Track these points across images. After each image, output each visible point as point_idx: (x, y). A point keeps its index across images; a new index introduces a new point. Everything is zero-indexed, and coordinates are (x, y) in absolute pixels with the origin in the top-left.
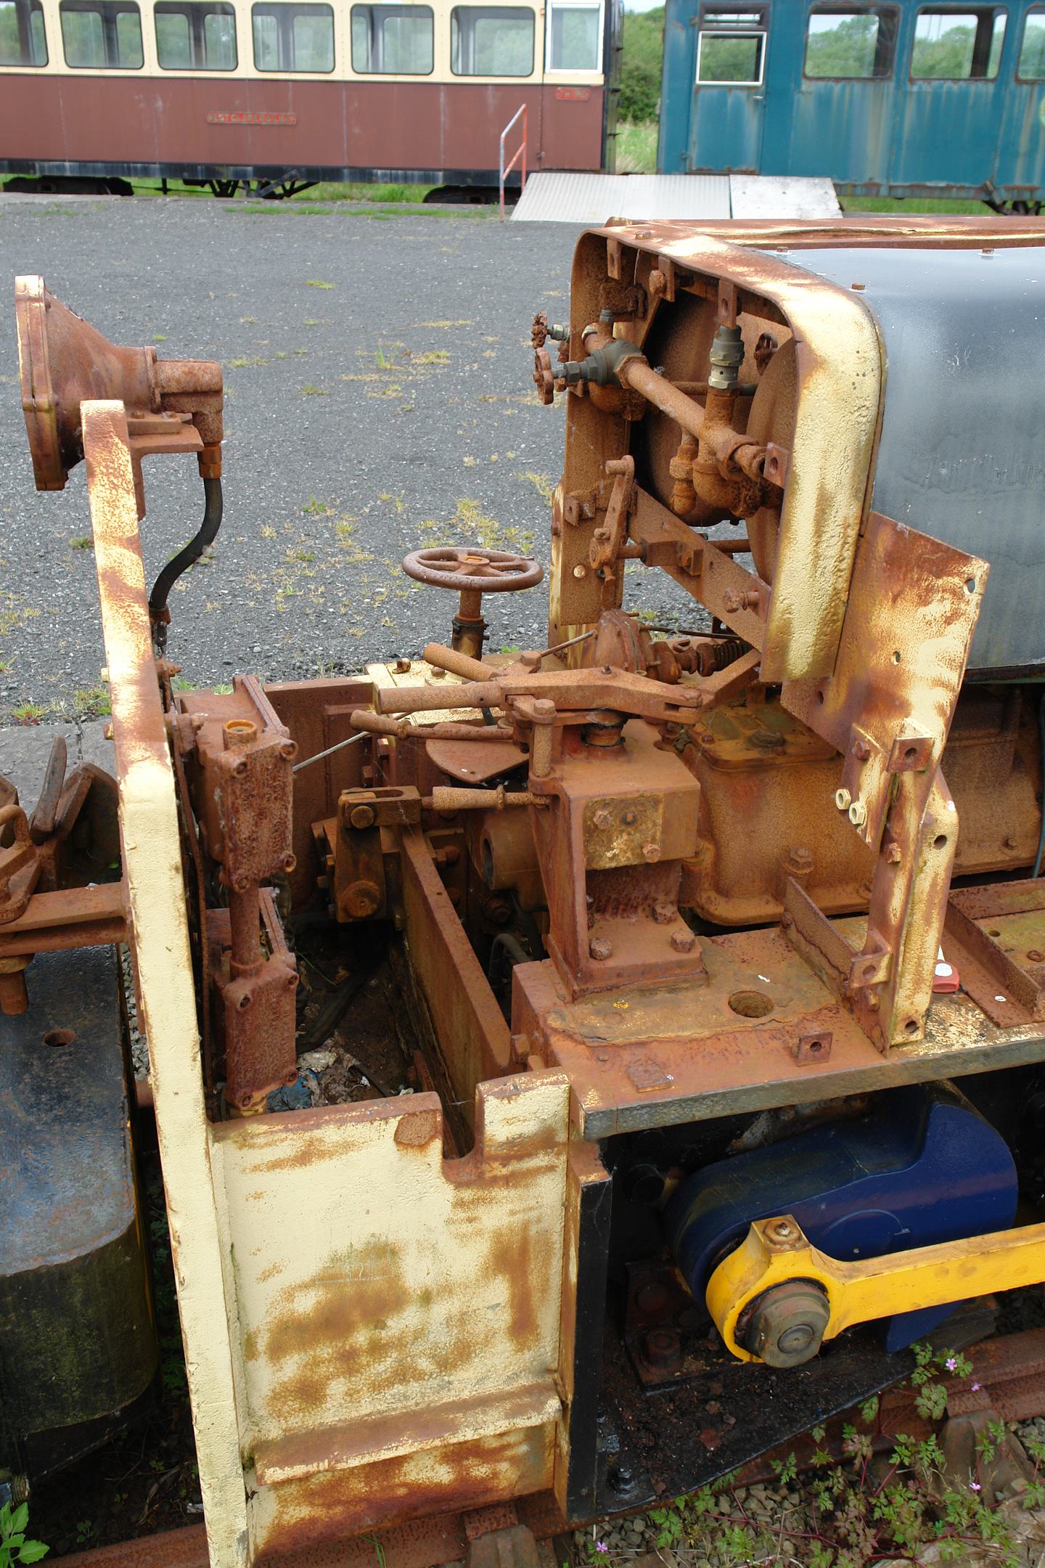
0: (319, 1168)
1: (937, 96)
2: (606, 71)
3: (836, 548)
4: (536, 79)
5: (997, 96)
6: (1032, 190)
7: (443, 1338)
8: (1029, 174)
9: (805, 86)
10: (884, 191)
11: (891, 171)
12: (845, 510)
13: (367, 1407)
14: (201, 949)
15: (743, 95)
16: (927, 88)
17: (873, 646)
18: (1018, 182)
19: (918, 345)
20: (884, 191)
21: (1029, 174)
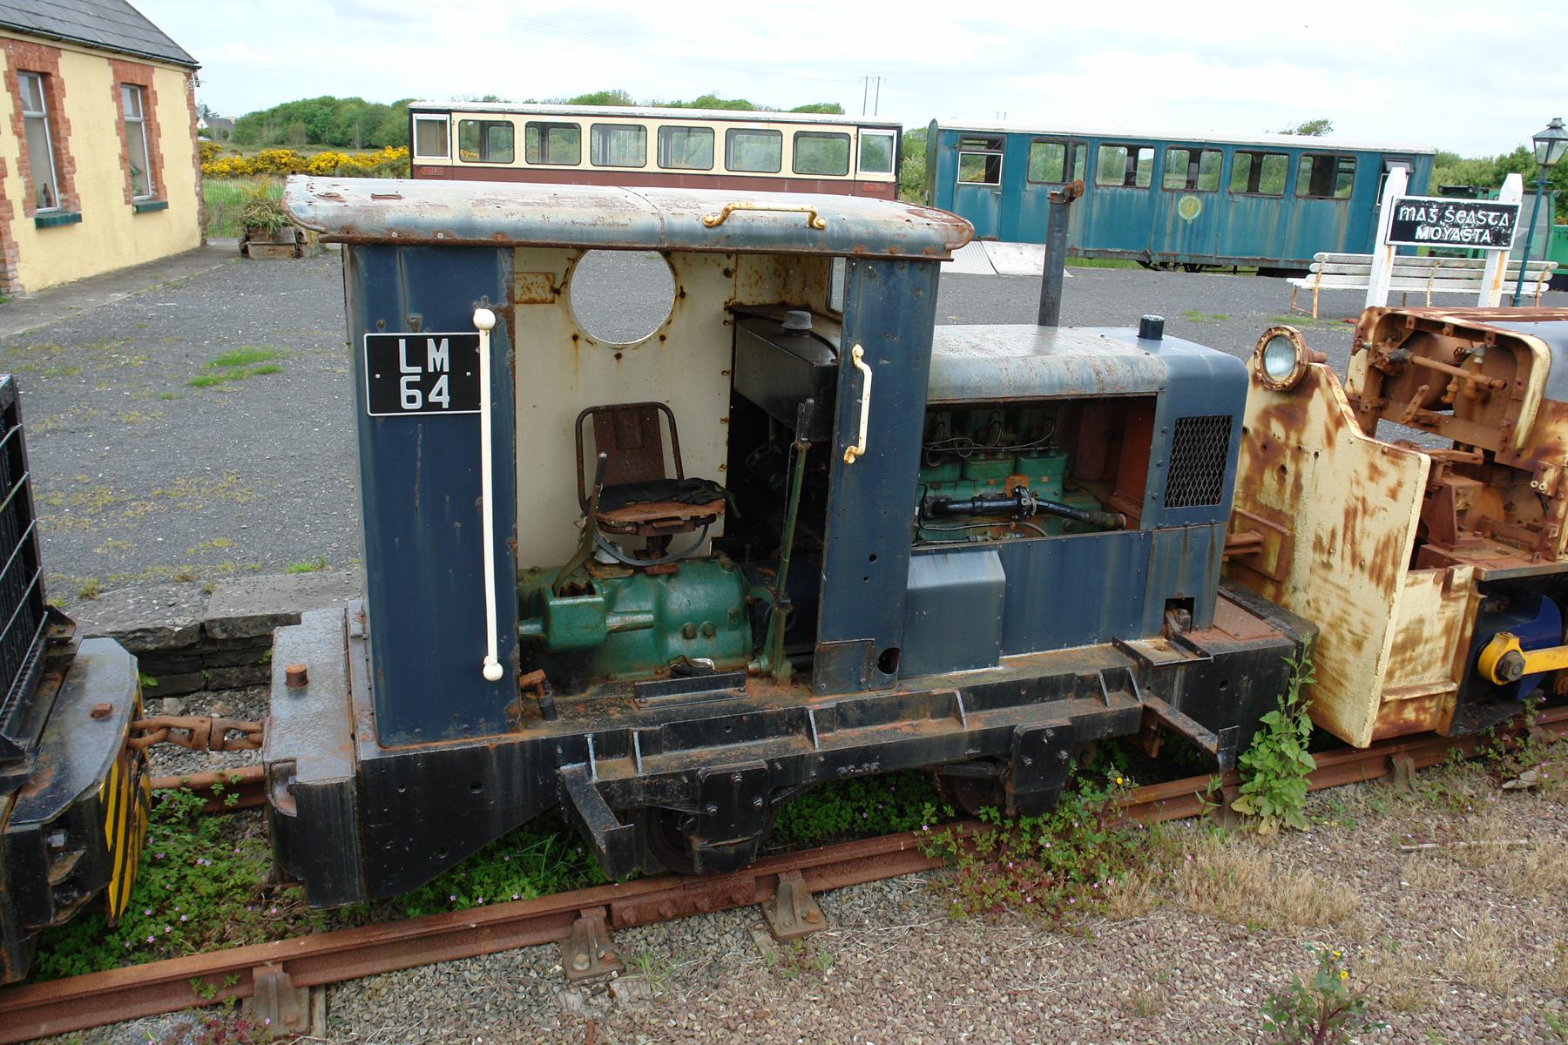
0: (1417, 587)
1: (1113, 196)
2: (897, 174)
3: (1534, 409)
4: (850, 177)
5: (1151, 197)
6: (1176, 256)
7: (1425, 658)
8: (1173, 247)
9: (1028, 187)
10: (1081, 253)
11: (1085, 241)
12: (1538, 397)
13: (1402, 684)
14: (875, 704)
15: (988, 191)
16: (1106, 191)
17: (1547, 436)
18: (1166, 250)
19: (1558, 352)
20: (1081, 253)
21: (1173, 247)
